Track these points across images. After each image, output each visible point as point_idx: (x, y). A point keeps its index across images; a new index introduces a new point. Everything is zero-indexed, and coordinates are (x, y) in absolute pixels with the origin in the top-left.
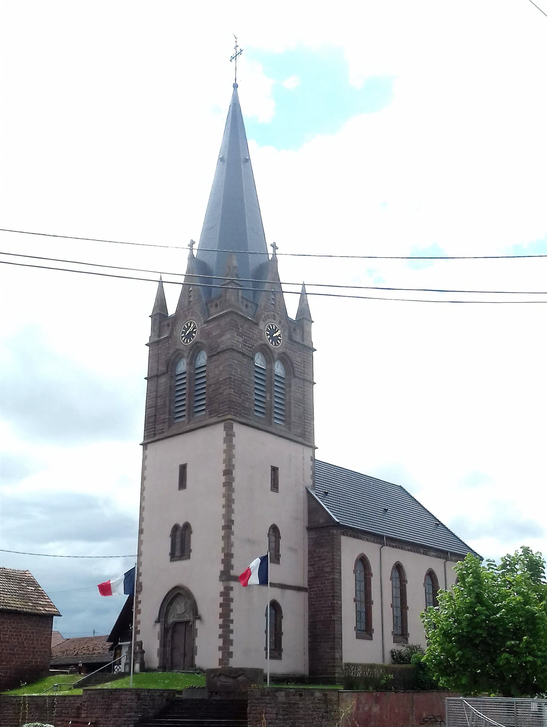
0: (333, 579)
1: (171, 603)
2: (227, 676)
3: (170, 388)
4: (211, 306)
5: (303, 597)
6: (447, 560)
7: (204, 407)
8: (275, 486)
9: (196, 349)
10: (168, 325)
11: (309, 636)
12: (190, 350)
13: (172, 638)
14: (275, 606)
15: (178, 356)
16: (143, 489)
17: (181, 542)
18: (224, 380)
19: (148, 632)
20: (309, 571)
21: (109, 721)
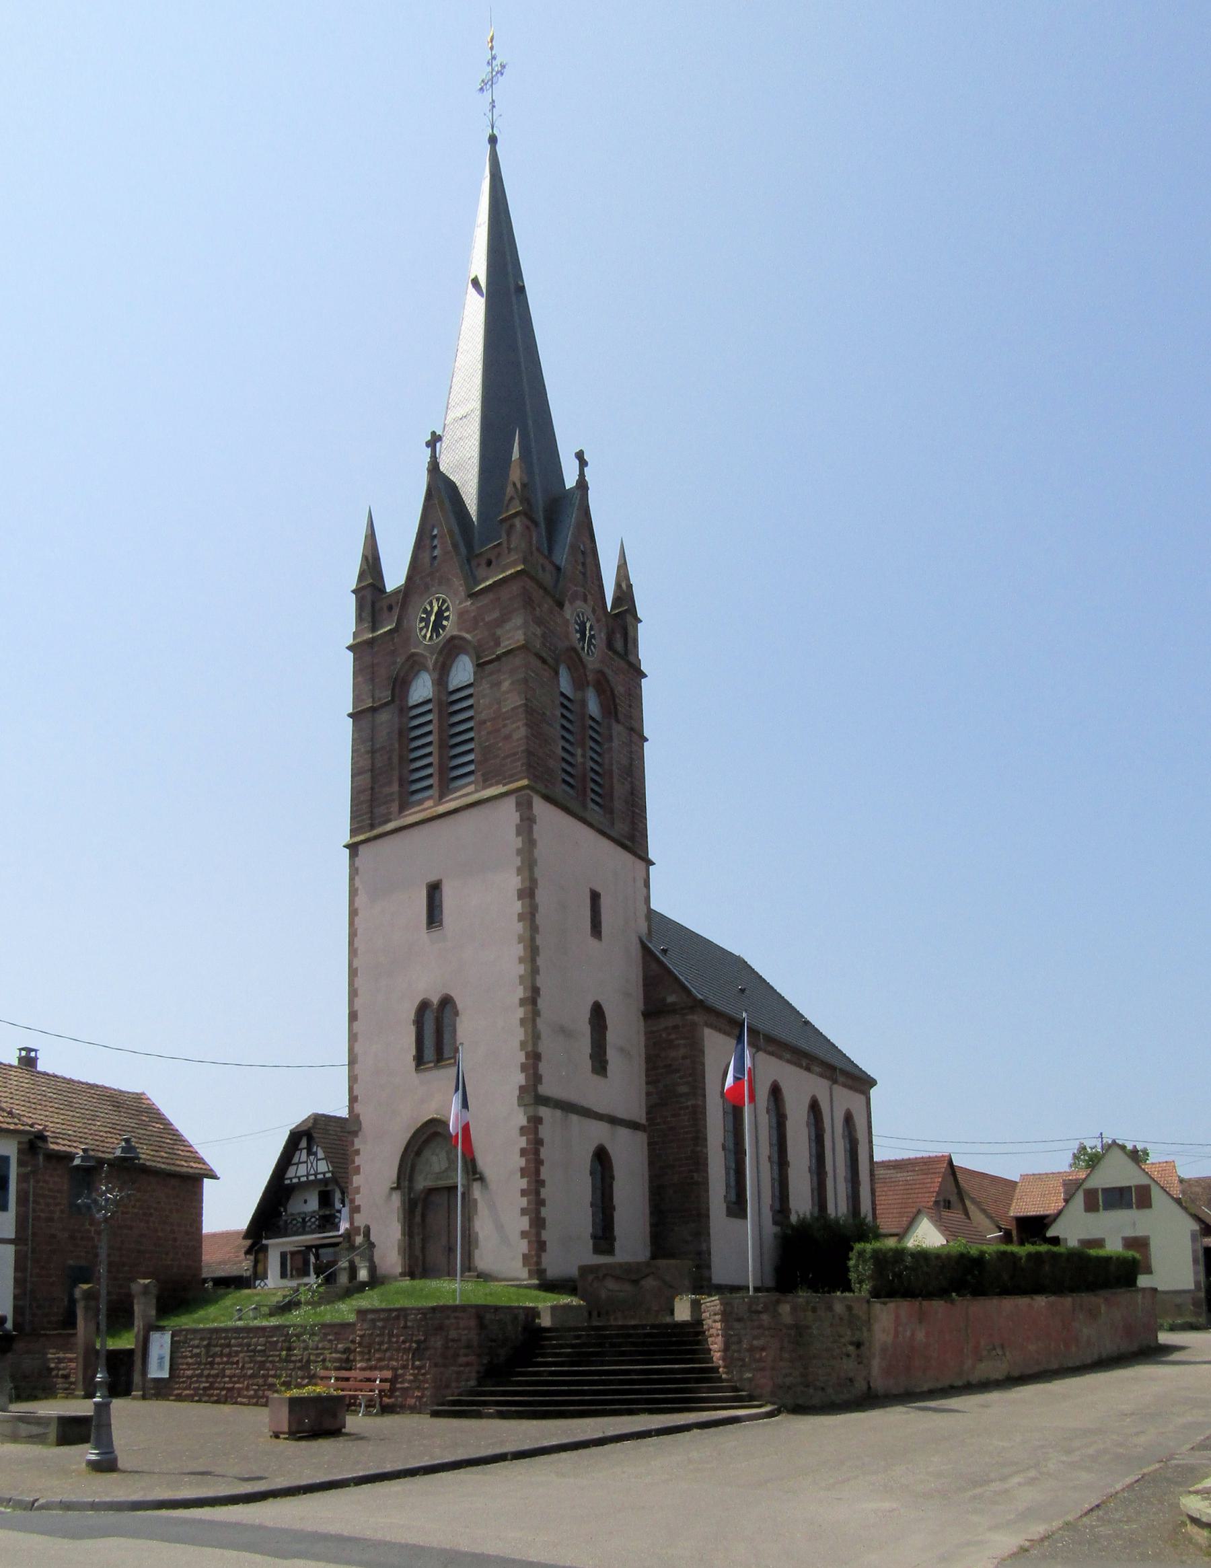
0: (694, 1106)
1: (418, 1153)
2: (617, 1278)
3: (401, 733)
4: (479, 565)
5: (641, 1138)
6: (835, 1081)
7: (472, 767)
8: (596, 928)
9: (451, 650)
10: (390, 608)
11: (652, 1213)
12: (440, 653)
13: (423, 1216)
14: (601, 1157)
15: (414, 665)
16: (353, 934)
17: (436, 1033)
18: (513, 709)
19: (376, 1210)
20: (648, 1094)
21: (423, 1375)
